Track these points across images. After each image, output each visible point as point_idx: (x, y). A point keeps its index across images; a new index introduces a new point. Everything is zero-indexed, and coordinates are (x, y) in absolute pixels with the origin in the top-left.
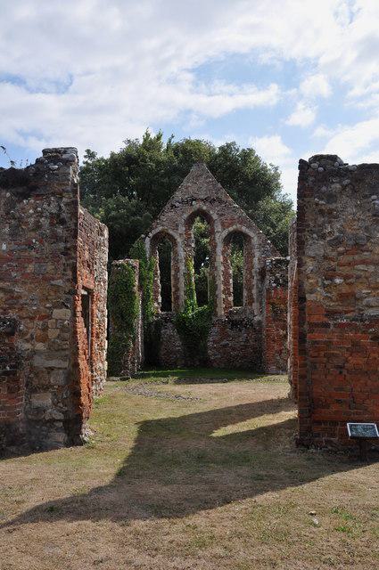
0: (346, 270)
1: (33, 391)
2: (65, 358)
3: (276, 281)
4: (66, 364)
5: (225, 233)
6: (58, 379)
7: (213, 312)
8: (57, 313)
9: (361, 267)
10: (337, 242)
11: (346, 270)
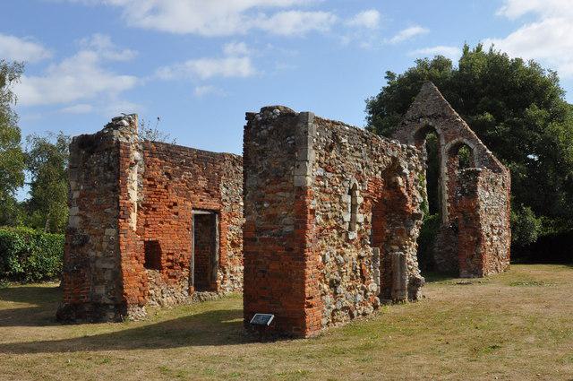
0: (271, 196)
1: (97, 284)
2: (111, 262)
3: (462, 191)
4: (112, 266)
5: (448, 147)
6: (108, 276)
7: (440, 220)
8: (108, 231)
9: (280, 194)
10: (265, 175)
11: (271, 196)
